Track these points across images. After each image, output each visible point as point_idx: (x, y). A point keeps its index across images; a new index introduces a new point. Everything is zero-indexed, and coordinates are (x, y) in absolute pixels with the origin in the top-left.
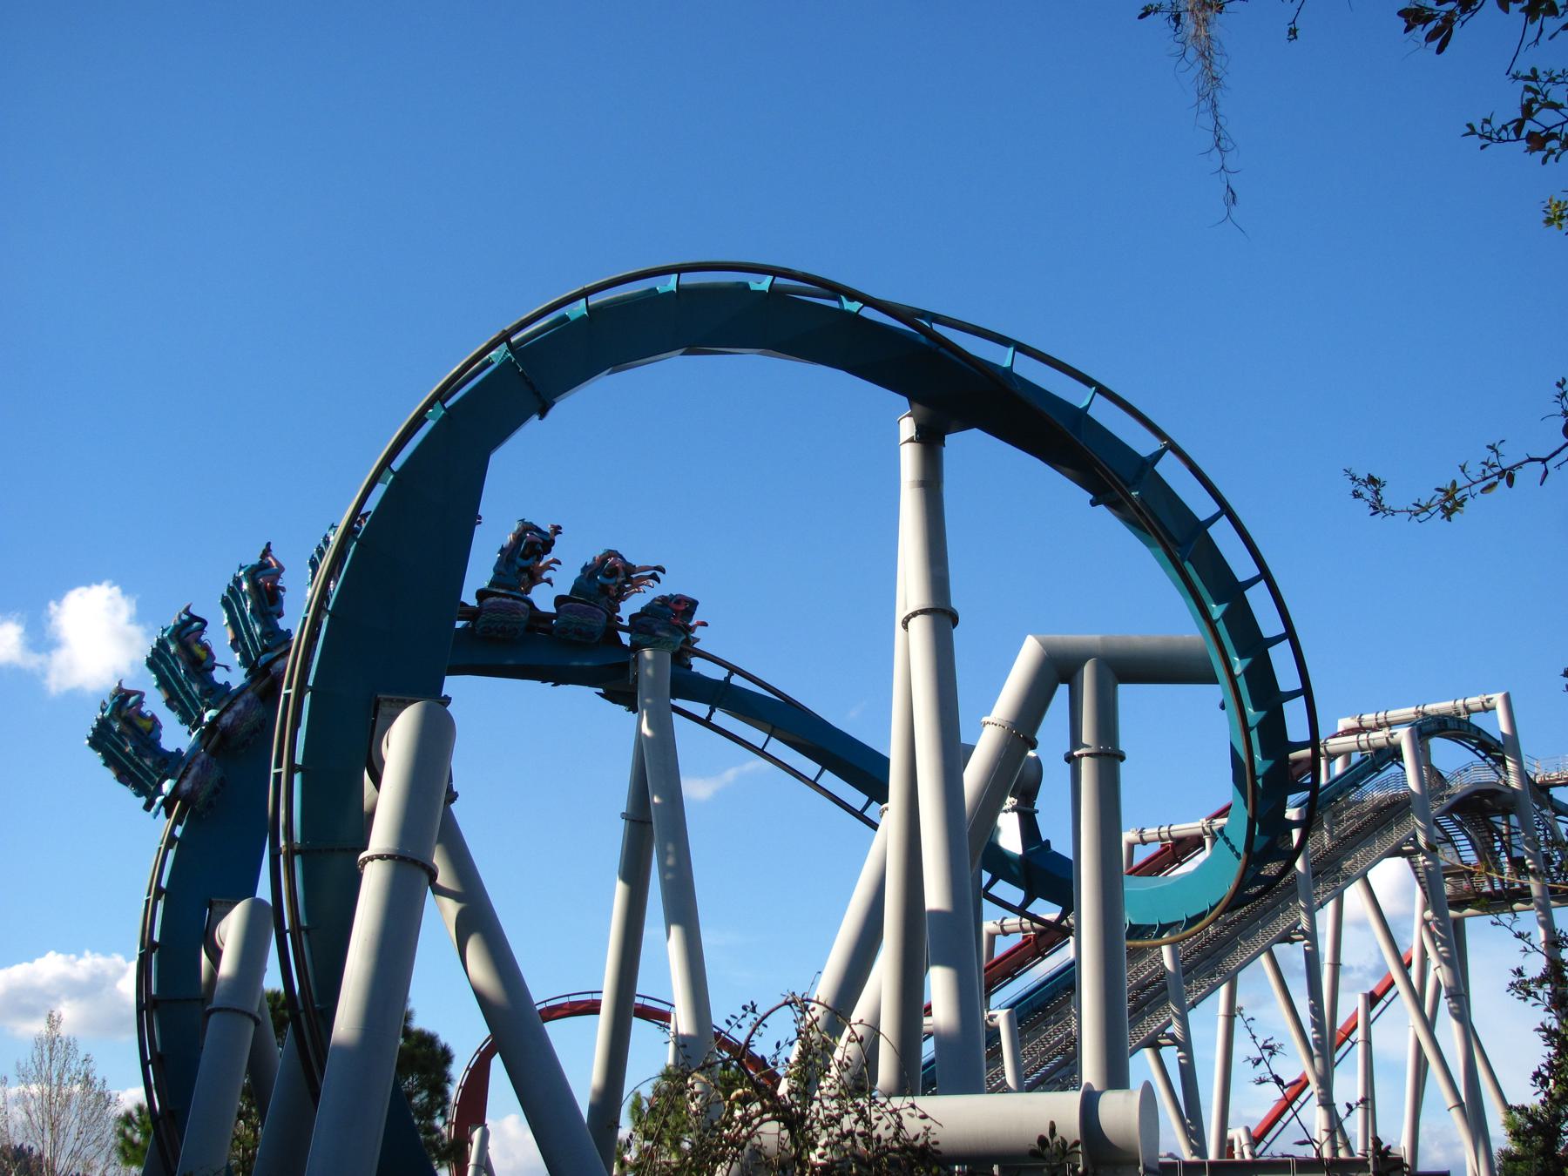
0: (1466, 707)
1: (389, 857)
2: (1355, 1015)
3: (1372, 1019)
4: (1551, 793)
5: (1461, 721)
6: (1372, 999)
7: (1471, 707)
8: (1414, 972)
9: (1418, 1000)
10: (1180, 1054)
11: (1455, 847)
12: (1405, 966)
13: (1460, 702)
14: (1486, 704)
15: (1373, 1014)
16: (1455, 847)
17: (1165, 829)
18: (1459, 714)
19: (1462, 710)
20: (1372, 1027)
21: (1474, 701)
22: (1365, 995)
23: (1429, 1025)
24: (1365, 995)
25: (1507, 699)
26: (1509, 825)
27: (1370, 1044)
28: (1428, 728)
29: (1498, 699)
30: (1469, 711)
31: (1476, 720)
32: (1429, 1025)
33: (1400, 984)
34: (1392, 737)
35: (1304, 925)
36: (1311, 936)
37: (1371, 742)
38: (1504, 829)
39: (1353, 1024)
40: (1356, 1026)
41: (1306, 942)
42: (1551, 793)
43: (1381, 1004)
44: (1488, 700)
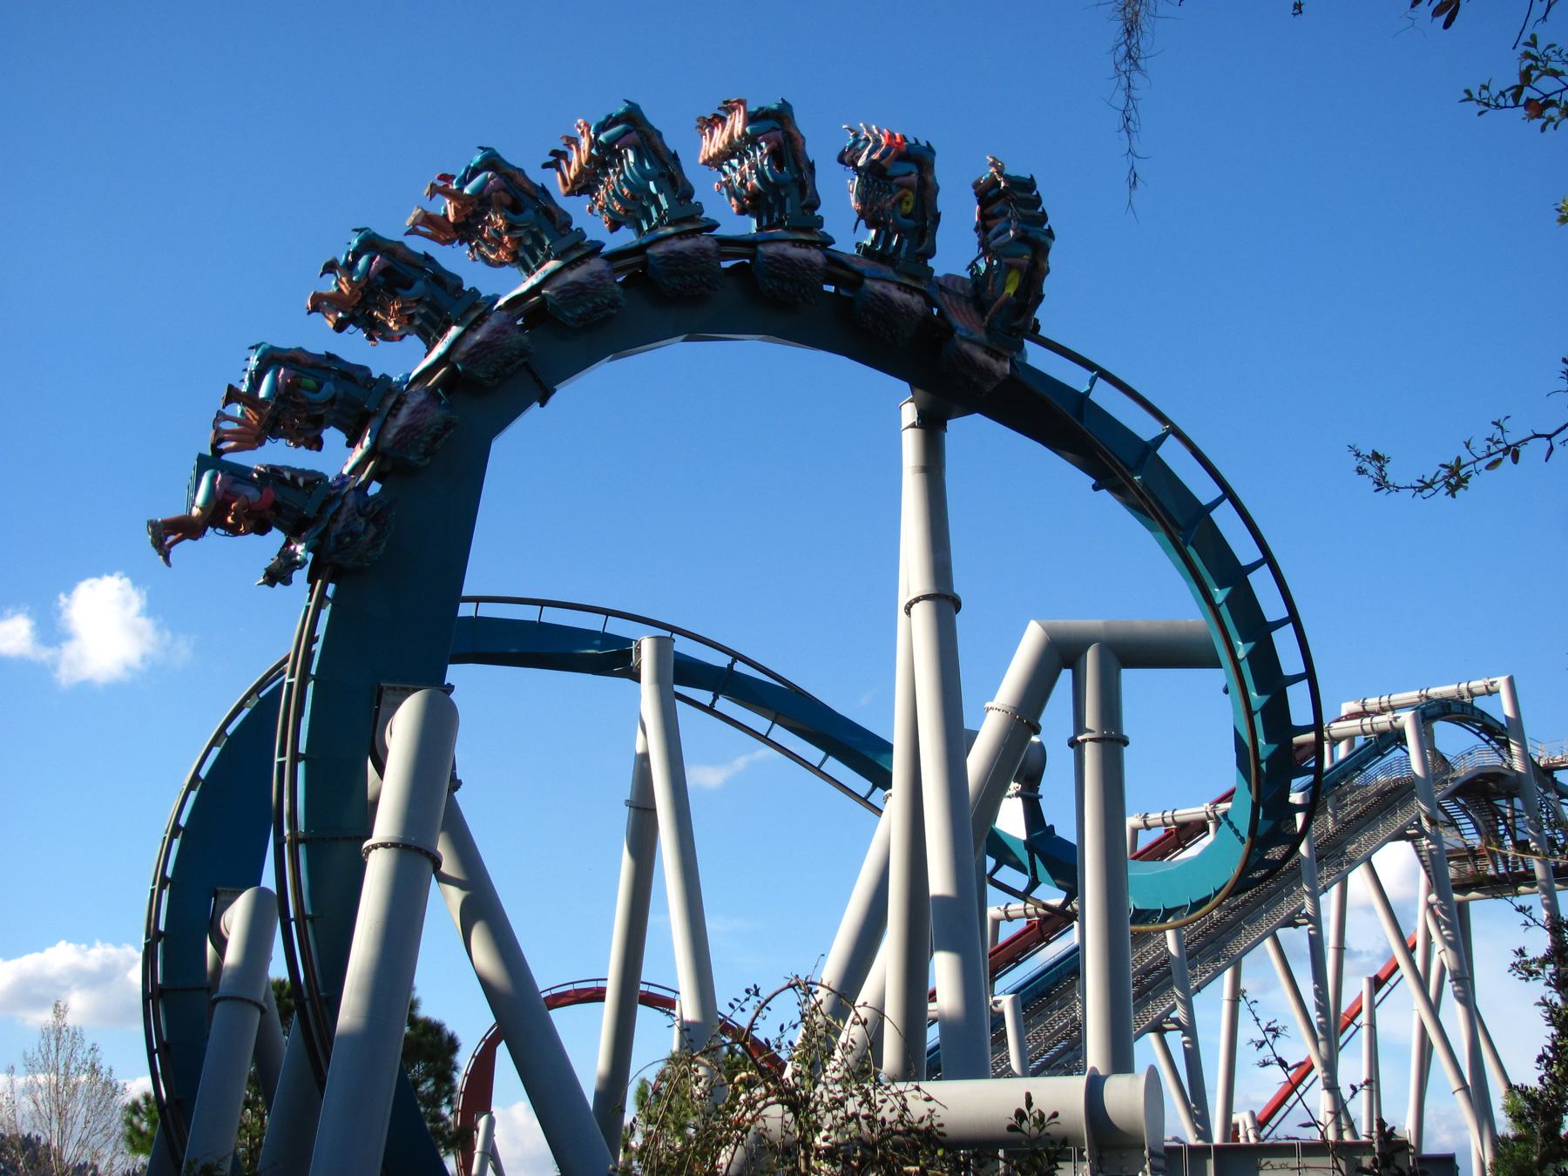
0: (1469, 690)
1: (393, 845)
2: (1360, 998)
3: (1376, 1002)
4: (1555, 776)
5: (1464, 704)
6: (1377, 983)
7: (1474, 690)
8: (1419, 956)
9: (1423, 983)
10: (1185, 1038)
11: (1459, 830)
12: (1409, 950)
13: (1463, 686)
14: (1489, 687)
15: (1377, 998)
16: (1459, 830)
17: (1168, 814)
18: (1463, 698)
19: (1466, 694)
20: (1378, 1011)
21: (1478, 685)
22: (1370, 979)
23: (1434, 1008)
24: (1370, 979)
25: (1511, 681)
26: (1513, 809)
27: (1375, 1027)
28: (1431, 712)
29: (1501, 683)
30: (1472, 695)
31: (1480, 703)
32: (1434, 1008)
33: (1404, 969)
34: (1396, 721)
35: (1308, 909)
36: (1316, 920)
37: (1375, 726)
38: (1508, 812)
39: (1357, 1008)
40: (1360, 1010)
41: (1310, 926)
42: (1555, 776)
43: (1386, 988)
44: (1492, 684)
